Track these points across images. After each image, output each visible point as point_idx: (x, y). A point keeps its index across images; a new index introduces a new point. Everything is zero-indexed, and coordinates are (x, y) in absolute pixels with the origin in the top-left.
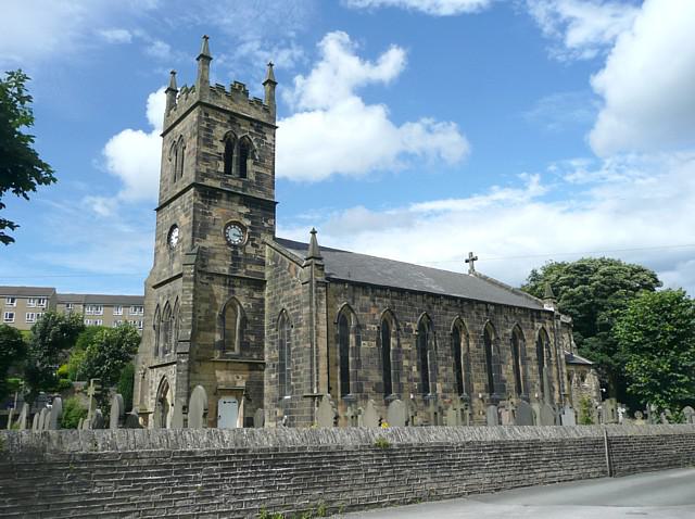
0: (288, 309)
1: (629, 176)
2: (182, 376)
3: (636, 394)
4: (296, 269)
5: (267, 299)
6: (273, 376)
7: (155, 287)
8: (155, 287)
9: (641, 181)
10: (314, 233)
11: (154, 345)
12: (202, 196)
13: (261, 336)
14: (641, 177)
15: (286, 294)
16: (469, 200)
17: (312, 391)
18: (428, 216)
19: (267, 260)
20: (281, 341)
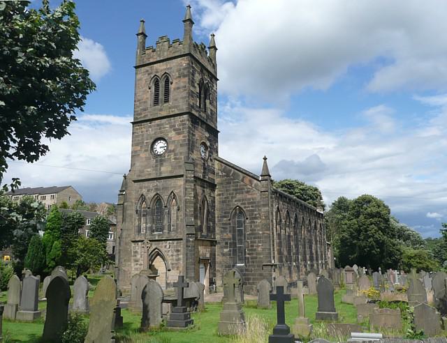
0: (242, 206)
1: (225, 120)
2: (191, 251)
3: (108, 233)
4: (250, 181)
5: (217, 198)
6: (225, 250)
7: (135, 181)
8: (135, 181)
9: (231, 124)
10: (265, 159)
11: (137, 224)
12: (192, 122)
13: (214, 223)
14: (231, 122)
15: (239, 196)
16: (124, 118)
17: (271, 262)
18: (95, 124)
19: (216, 171)
20: (234, 227)
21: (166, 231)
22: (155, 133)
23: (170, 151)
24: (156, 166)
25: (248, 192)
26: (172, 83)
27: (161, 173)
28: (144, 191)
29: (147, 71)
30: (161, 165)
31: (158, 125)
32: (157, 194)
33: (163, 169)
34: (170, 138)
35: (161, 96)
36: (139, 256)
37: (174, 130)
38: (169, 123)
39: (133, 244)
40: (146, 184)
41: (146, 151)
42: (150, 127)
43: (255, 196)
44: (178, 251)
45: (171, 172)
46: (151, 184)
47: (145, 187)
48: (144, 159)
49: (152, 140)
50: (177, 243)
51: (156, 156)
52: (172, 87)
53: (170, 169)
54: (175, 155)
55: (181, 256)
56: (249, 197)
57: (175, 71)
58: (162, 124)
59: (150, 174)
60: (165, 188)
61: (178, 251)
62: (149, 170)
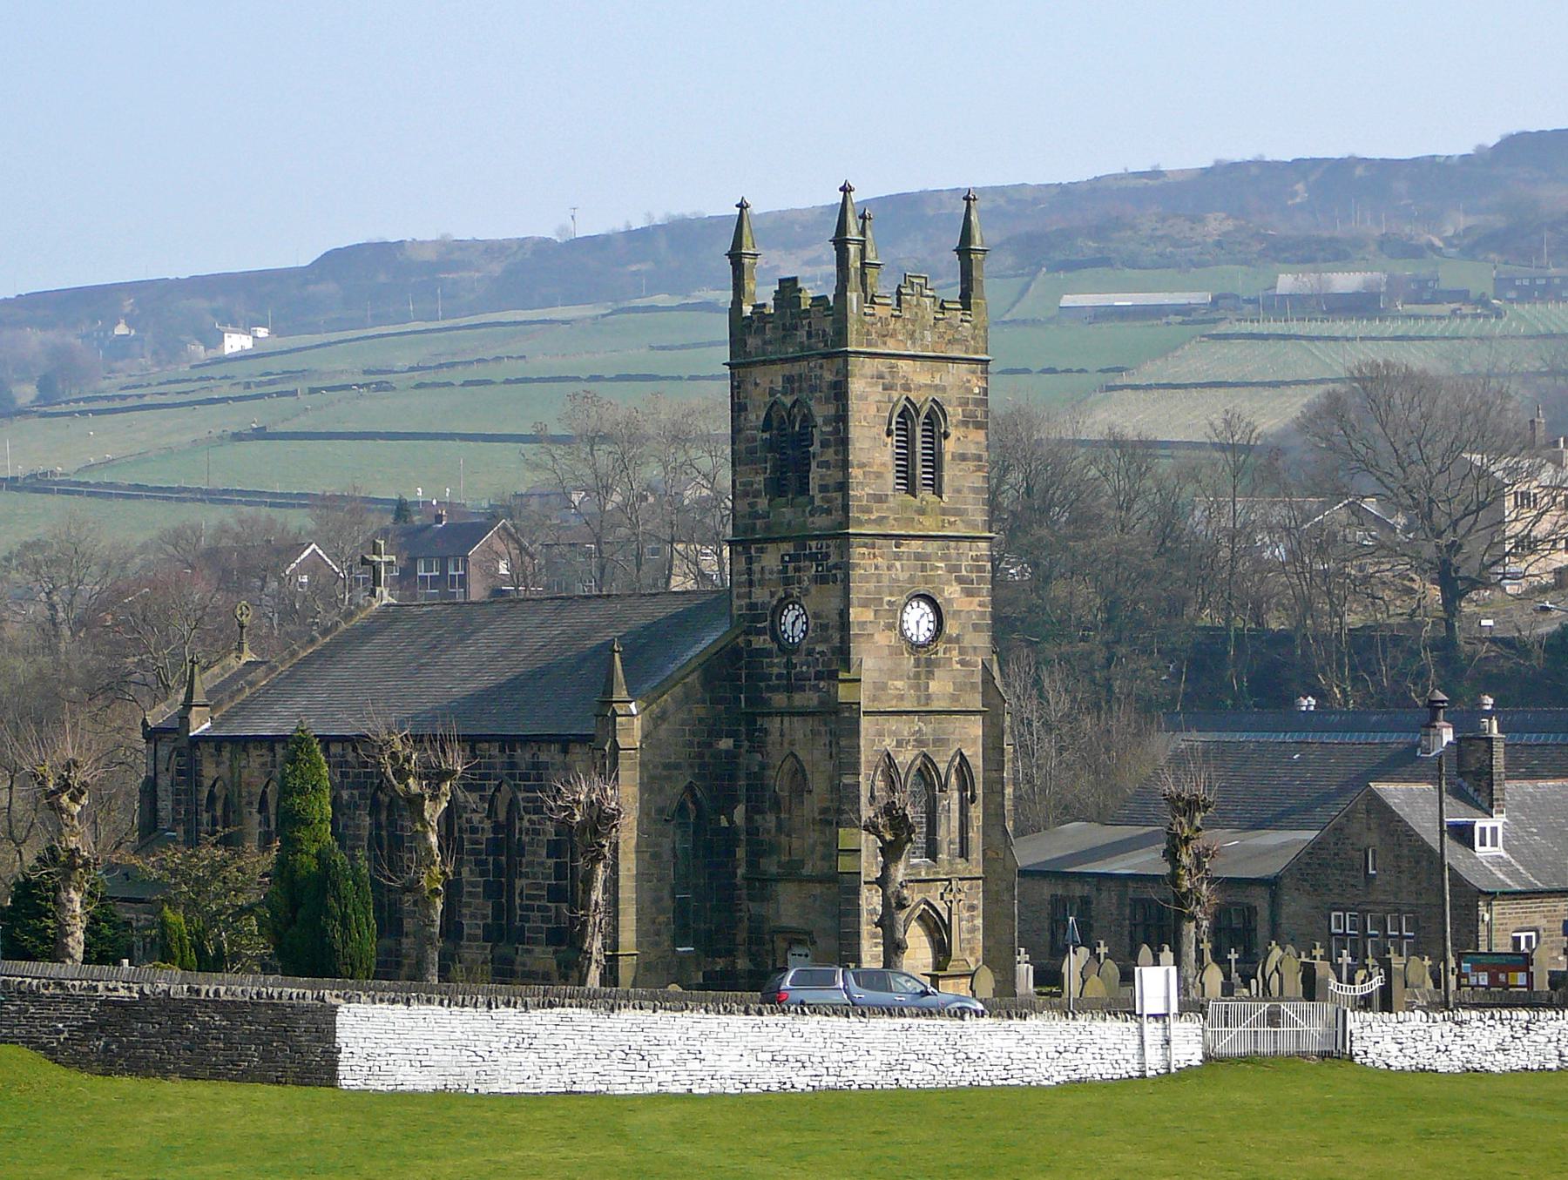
21: (943, 856)
22: (911, 579)
23: (950, 640)
24: (917, 676)
27: (928, 697)
31: (918, 556)
32: (925, 755)
34: (949, 601)
37: (960, 580)
38: (945, 558)
40: (893, 723)
42: (898, 557)
46: (905, 727)
47: (893, 733)
48: (886, 651)
50: (971, 888)
54: (962, 651)
55: (979, 922)
57: (955, 402)
58: (927, 557)
62: (899, 684)
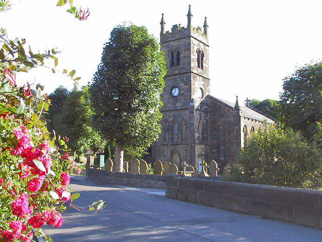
4: (228, 111)
15: (222, 119)
25: (227, 117)
26: (181, 53)
28: (167, 117)
29: (166, 46)
30: (177, 103)
33: (177, 105)
35: (175, 55)
36: (165, 153)
39: (162, 146)
41: (168, 94)
42: (169, 80)
43: (230, 119)
44: (186, 151)
45: (182, 106)
49: (170, 88)
51: (173, 97)
52: (182, 56)
53: (181, 104)
56: (227, 119)
59: (170, 108)
60: (179, 116)
61: (186, 151)
62: (170, 105)
